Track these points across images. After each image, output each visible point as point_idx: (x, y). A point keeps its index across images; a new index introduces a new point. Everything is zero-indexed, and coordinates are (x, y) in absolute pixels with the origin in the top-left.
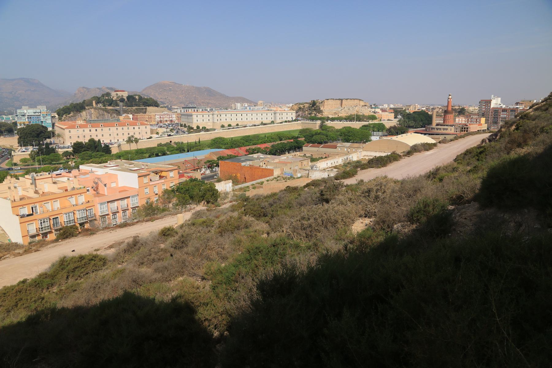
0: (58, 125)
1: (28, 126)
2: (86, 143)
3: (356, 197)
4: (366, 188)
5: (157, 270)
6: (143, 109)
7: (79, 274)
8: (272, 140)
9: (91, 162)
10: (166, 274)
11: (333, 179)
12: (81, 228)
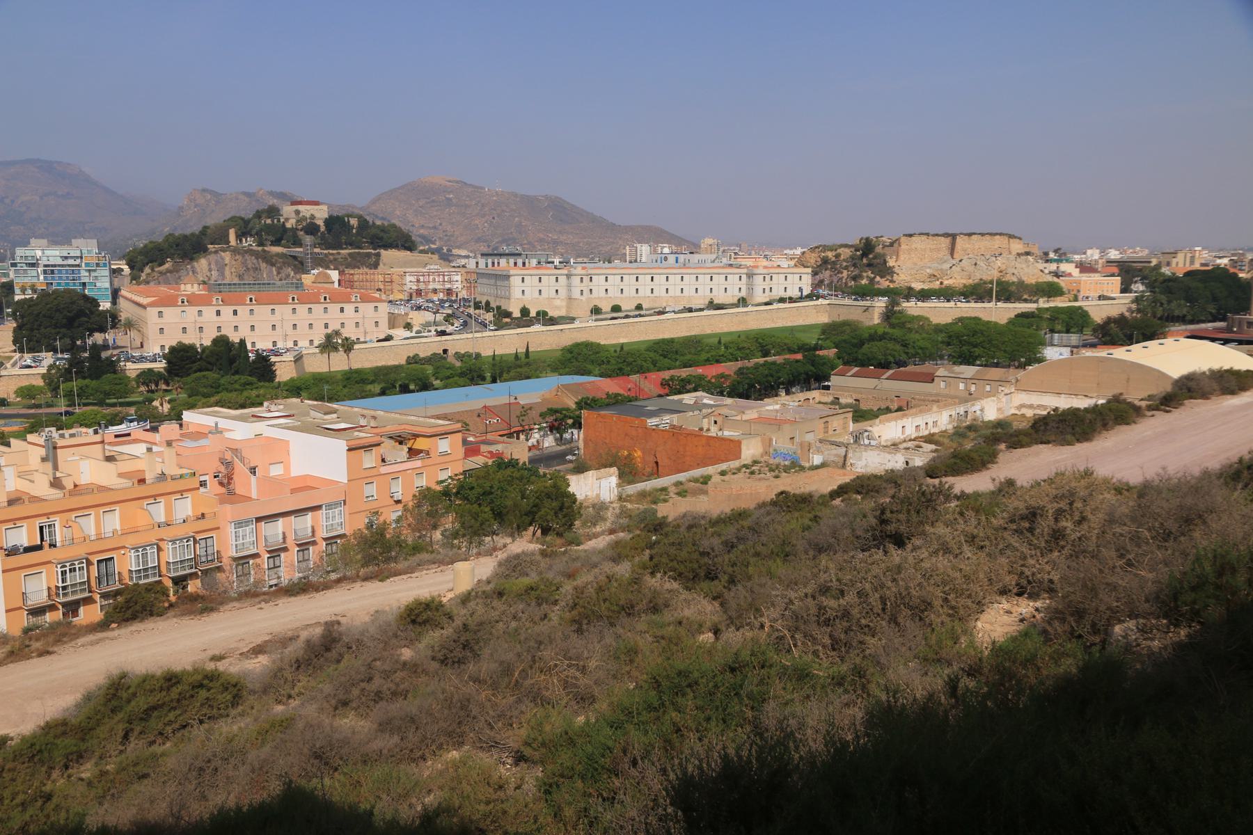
0: (129, 295)
1: (44, 294)
2: (204, 349)
3: (990, 532)
4: (1021, 505)
5: (385, 726)
6: (369, 255)
7: (160, 726)
8: (739, 354)
9: (217, 404)
10: (413, 737)
11: (922, 473)
12: (176, 592)
